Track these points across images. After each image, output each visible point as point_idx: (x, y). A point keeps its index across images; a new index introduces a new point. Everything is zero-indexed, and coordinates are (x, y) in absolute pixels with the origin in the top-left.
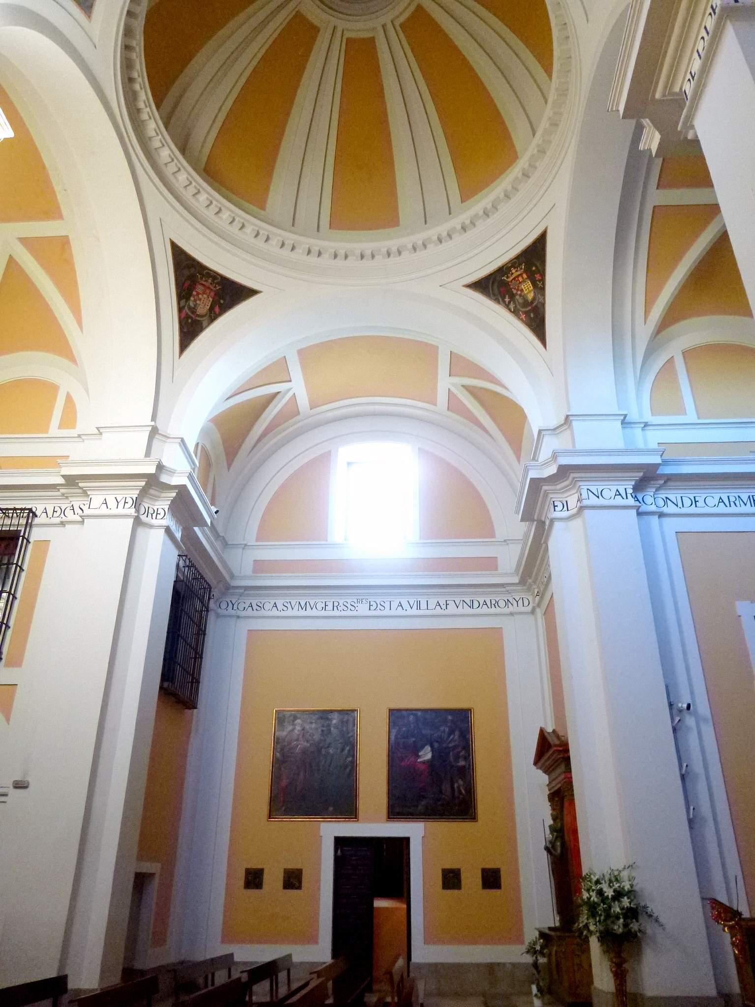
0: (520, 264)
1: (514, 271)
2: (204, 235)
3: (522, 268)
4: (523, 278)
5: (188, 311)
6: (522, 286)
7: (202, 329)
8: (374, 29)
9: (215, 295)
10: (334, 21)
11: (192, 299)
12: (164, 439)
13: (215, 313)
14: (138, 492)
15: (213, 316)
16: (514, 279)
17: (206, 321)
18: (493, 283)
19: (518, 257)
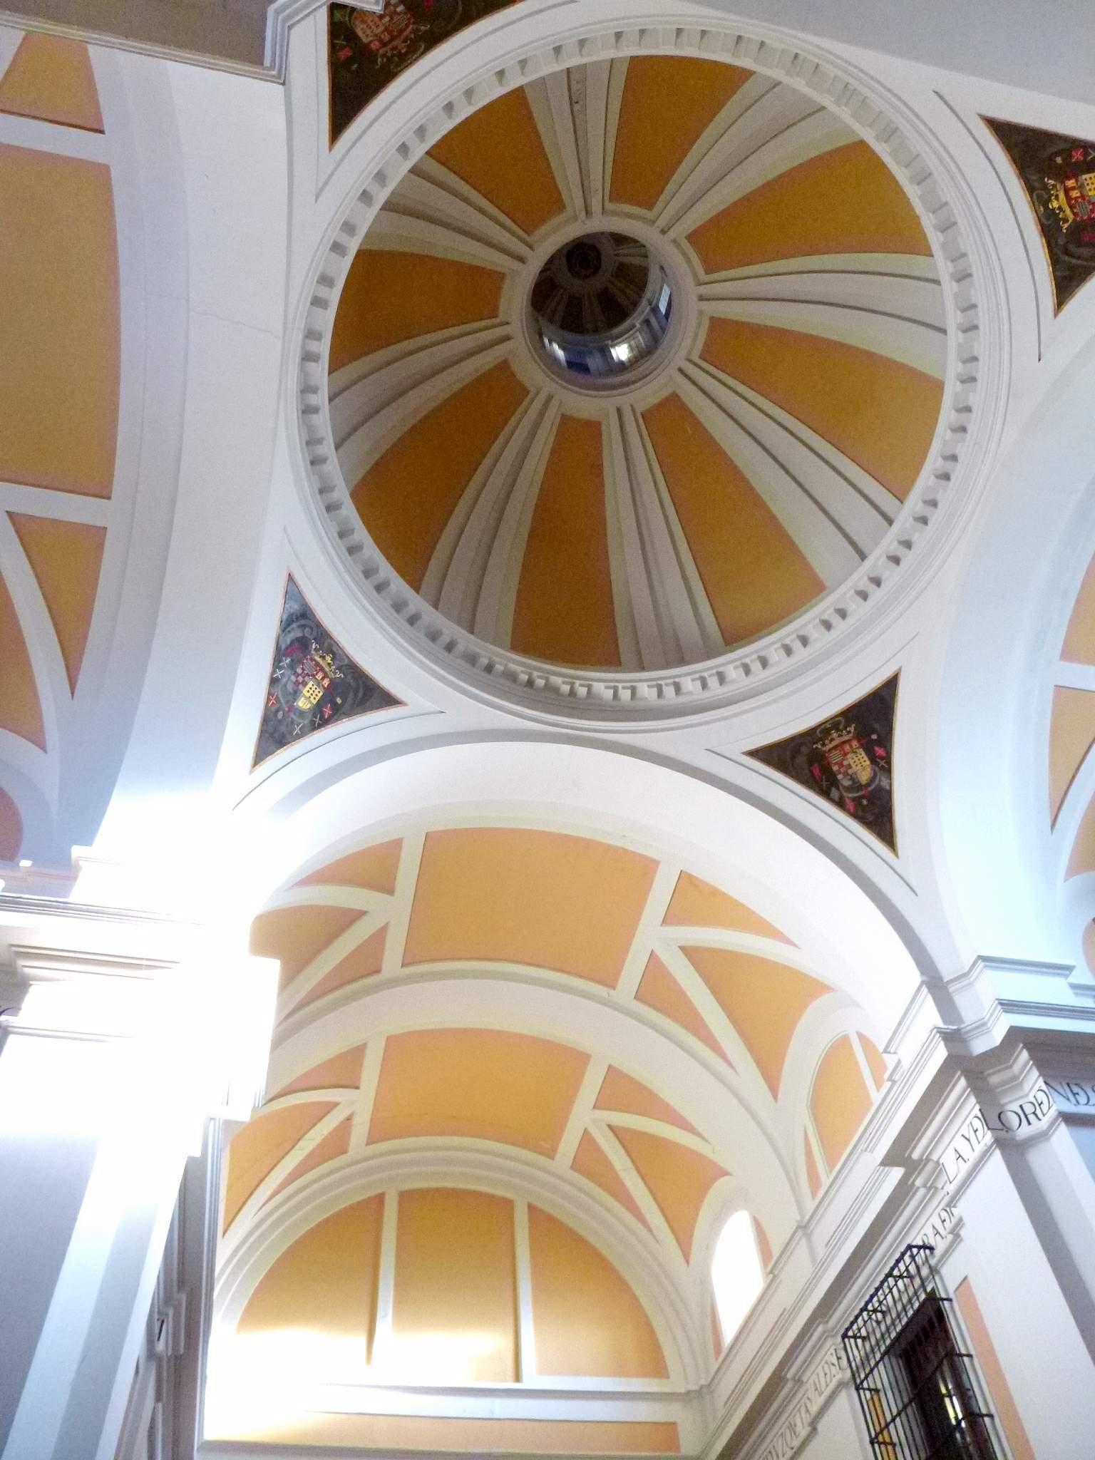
0: (1045, 187)
1: (1055, 204)
2: (768, 704)
3: (1054, 186)
4: (1073, 188)
5: (850, 795)
6: (1090, 194)
7: (889, 794)
8: (701, 313)
9: (859, 741)
10: (672, 371)
11: (840, 777)
12: (965, 982)
13: (882, 758)
14: (973, 1100)
15: (883, 764)
16: (1071, 207)
17: (883, 779)
18: (1072, 255)
19: (1030, 189)
